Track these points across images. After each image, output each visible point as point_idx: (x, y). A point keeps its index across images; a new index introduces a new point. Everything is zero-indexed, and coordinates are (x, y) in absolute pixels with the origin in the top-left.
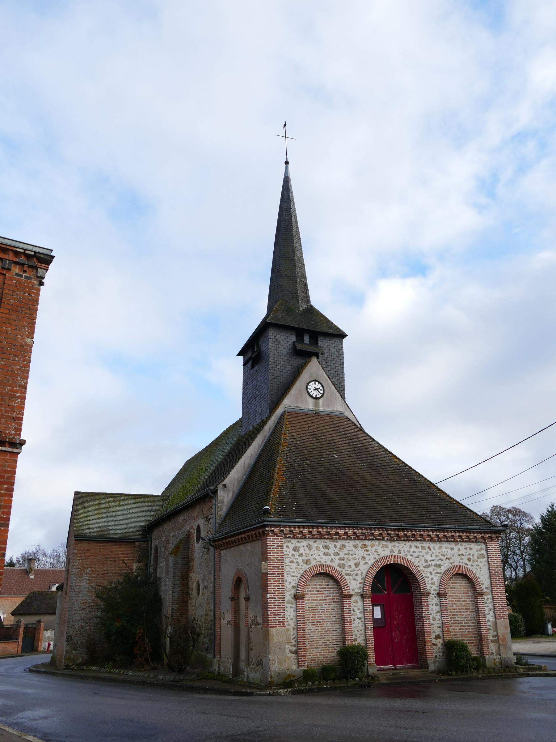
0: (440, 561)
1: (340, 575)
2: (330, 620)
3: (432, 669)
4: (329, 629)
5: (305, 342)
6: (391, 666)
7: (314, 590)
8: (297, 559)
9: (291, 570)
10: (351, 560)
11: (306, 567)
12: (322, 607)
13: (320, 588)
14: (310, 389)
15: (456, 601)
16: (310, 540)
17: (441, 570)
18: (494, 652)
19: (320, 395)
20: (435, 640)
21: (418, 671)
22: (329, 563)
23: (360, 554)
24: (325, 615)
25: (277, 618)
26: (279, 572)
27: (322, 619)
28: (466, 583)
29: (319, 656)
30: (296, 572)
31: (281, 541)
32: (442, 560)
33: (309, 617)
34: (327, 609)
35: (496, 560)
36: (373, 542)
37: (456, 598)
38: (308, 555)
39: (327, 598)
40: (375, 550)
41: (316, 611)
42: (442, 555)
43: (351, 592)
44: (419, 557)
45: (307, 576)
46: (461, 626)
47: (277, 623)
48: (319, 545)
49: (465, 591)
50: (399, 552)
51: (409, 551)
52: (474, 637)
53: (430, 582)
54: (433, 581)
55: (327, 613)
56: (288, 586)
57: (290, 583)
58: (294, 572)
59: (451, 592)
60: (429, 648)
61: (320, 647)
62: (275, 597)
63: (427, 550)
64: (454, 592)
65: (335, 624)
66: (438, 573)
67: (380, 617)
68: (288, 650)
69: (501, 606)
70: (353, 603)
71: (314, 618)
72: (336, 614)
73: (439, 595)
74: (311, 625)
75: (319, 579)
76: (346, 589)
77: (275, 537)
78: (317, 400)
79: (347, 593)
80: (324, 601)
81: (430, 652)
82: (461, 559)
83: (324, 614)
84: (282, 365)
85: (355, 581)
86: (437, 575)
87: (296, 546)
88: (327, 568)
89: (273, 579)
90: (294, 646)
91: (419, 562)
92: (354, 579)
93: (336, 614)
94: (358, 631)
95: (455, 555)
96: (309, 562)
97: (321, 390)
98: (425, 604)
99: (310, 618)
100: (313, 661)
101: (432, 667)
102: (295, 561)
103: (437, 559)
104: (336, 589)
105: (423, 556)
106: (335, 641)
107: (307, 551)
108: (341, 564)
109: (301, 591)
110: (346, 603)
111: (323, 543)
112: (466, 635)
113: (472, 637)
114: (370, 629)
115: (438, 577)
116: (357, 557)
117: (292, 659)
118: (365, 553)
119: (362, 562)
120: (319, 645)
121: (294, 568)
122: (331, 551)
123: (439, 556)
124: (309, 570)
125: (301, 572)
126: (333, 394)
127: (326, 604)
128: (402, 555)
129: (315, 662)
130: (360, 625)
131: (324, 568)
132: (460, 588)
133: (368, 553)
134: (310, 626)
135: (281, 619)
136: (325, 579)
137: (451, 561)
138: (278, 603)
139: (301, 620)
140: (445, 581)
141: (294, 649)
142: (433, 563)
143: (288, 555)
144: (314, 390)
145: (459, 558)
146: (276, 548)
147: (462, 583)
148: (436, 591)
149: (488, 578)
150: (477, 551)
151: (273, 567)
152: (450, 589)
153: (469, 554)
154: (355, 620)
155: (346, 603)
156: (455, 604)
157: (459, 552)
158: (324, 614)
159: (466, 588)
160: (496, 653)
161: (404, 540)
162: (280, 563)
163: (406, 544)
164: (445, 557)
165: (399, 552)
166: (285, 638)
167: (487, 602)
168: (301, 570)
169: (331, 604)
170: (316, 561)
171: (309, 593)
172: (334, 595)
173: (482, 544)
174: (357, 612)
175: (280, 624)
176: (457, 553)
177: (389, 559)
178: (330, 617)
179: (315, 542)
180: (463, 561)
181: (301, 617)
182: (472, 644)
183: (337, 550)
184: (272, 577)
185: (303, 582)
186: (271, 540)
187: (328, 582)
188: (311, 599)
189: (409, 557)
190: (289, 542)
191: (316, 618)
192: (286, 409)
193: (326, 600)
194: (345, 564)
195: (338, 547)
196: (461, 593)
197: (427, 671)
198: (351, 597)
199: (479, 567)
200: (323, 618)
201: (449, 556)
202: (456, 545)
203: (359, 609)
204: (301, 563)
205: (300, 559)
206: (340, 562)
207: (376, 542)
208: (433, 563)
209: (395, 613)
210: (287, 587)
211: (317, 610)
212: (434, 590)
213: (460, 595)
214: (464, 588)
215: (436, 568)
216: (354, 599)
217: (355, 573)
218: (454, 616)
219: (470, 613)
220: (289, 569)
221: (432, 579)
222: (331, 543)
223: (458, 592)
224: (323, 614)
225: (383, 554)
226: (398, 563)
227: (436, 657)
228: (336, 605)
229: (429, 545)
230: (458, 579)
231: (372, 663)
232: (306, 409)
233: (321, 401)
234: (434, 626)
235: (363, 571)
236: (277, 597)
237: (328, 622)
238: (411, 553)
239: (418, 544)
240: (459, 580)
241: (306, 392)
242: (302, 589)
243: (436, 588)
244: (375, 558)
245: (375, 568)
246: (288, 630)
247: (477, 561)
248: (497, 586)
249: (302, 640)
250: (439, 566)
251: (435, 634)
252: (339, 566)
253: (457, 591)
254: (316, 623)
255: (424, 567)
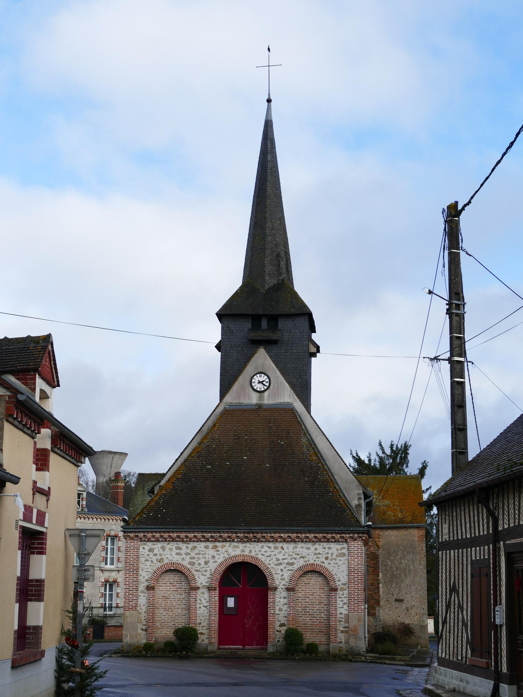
0: (294, 559)
1: (189, 572)
2: (180, 607)
3: (270, 651)
4: (179, 614)
5: (262, 327)
6: (241, 647)
7: (168, 583)
8: (152, 558)
9: (146, 567)
10: (201, 559)
11: (159, 565)
12: (174, 597)
13: (173, 581)
14: (254, 382)
15: (309, 595)
16: (164, 542)
17: (293, 567)
18: (343, 641)
19: (266, 388)
20: (279, 627)
21: (260, 652)
22: (180, 561)
23: (210, 554)
24: (176, 603)
25: (131, 604)
26: (134, 568)
27: (173, 606)
28: (322, 579)
29: (168, 634)
30: (149, 569)
31: (136, 544)
32: (295, 559)
33: (162, 604)
34: (178, 599)
35: (357, 558)
36: (224, 543)
37: (309, 593)
38: (162, 554)
39: (179, 590)
40: (225, 551)
41: (168, 600)
42: (296, 554)
43: (198, 585)
44: (271, 556)
45: (158, 572)
46: (312, 617)
47: (131, 608)
48: (171, 547)
49: (321, 586)
50: (251, 551)
51: (260, 551)
52: (326, 627)
53: (280, 578)
54: (283, 577)
55: (178, 601)
56: (141, 579)
57: (144, 577)
58: (148, 569)
59: (305, 587)
60: (271, 634)
61: (170, 627)
62: (130, 588)
63: (280, 550)
64: (308, 587)
65: (184, 610)
66: (289, 570)
67: (233, 606)
68: (139, 628)
69: (356, 601)
70: (200, 594)
71: (166, 605)
72: (186, 602)
73: (288, 589)
74: (164, 610)
75: (173, 574)
76: (193, 582)
77: (132, 541)
78: (262, 394)
79: (194, 586)
80: (176, 592)
81: (271, 637)
82: (318, 558)
83: (175, 602)
84: (234, 357)
85: (204, 576)
86: (288, 572)
87: (151, 547)
88: (177, 565)
89: (128, 574)
90: (145, 625)
91: (270, 561)
92: (203, 575)
93: (186, 602)
94: (203, 616)
95: (310, 554)
96: (162, 561)
97: (267, 382)
98: (271, 597)
99: (163, 605)
100: (162, 638)
101: (270, 649)
102: (149, 559)
103: (290, 558)
104: (187, 583)
105: (275, 555)
106: (183, 624)
107: (161, 551)
108: (190, 562)
109: (152, 583)
110: (192, 594)
111: (176, 545)
112: (317, 625)
113: (323, 627)
114: (213, 615)
115: (290, 573)
116: (207, 556)
117: (142, 635)
118: (216, 553)
119: (212, 561)
120: (169, 626)
121: (148, 565)
122: (183, 551)
123: (292, 555)
124: (161, 567)
125: (155, 568)
126: (281, 385)
127: (178, 594)
128: (253, 554)
129: (165, 639)
130: (206, 612)
131: (174, 566)
132: (316, 584)
133: (218, 553)
134: (162, 611)
135: (134, 604)
136: (178, 575)
137: (305, 559)
138: (132, 592)
139: (151, 606)
140: (295, 577)
141: (144, 628)
142: (285, 561)
143: (144, 555)
144: (258, 383)
145: (315, 556)
146: (132, 550)
147: (319, 579)
148: (286, 585)
149: (346, 575)
150: (337, 550)
151: (129, 564)
152: (304, 584)
153: (328, 553)
154: (201, 608)
155: (192, 594)
156: (308, 597)
157: (315, 551)
158: (175, 602)
159: (322, 584)
160: (345, 642)
161: (255, 541)
162: (135, 562)
163: (257, 545)
164: (300, 556)
165: (251, 551)
166: (136, 619)
167: (342, 597)
168: (154, 567)
169: (182, 595)
170: (168, 560)
171: (163, 585)
172: (186, 587)
173: (344, 543)
174: (204, 601)
175: (133, 609)
176: (313, 552)
177: (238, 558)
178: (181, 604)
179: (169, 544)
180: (319, 559)
181: (151, 604)
182: (323, 633)
183: (188, 551)
184: (128, 573)
185: (155, 576)
186: (129, 543)
187: (181, 577)
188: (164, 590)
189: (260, 557)
190: (145, 544)
191: (168, 605)
192: (227, 406)
193: (178, 591)
194: (195, 563)
195: (190, 548)
196: (315, 588)
197: (265, 652)
198: (197, 589)
199: (337, 565)
200: (174, 605)
201: (303, 555)
202: (314, 545)
203: (205, 599)
204: (155, 561)
205: (154, 559)
206: (190, 560)
207: (226, 544)
208: (285, 561)
209: (249, 604)
210: (141, 580)
211: (169, 599)
212: (284, 585)
213: (315, 590)
214: (319, 584)
215: (288, 566)
216: (202, 591)
217: (204, 569)
218: (305, 608)
219: (323, 606)
220: (144, 566)
221: (282, 575)
222: (183, 545)
223: (312, 587)
224: (174, 602)
225: (233, 554)
226: (246, 562)
227: (278, 641)
228: (187, 595)
229: (283, 545)
230: (314, 576)
231: (213, 643)
232: (249, 404)
233: (266, 394)
234: (280, 616)
235: (212, 568)
236: (131, 588)
237: (179, 608)
238: (262, 553)
239: (271, 545)
240: (316, 577)
241: (250, 387)
242: (153, 582)
243: (286, 584)
244: (224, 557)
245: (223, 566)
246: (140, 613)
247: (336, 560)
248: (355, 583)
249: (151, 621)
250: (292, 564)
251: (280, 622)
252: (189, 563)
253: (311, 586)
254: (167, 609)
255: (275, 565)
